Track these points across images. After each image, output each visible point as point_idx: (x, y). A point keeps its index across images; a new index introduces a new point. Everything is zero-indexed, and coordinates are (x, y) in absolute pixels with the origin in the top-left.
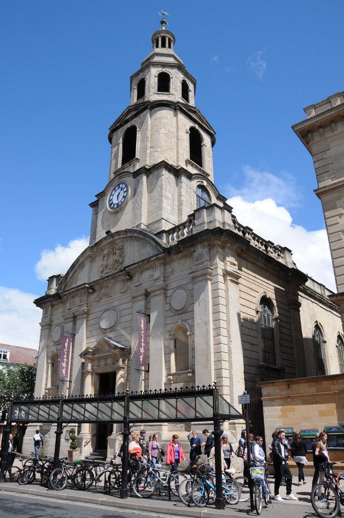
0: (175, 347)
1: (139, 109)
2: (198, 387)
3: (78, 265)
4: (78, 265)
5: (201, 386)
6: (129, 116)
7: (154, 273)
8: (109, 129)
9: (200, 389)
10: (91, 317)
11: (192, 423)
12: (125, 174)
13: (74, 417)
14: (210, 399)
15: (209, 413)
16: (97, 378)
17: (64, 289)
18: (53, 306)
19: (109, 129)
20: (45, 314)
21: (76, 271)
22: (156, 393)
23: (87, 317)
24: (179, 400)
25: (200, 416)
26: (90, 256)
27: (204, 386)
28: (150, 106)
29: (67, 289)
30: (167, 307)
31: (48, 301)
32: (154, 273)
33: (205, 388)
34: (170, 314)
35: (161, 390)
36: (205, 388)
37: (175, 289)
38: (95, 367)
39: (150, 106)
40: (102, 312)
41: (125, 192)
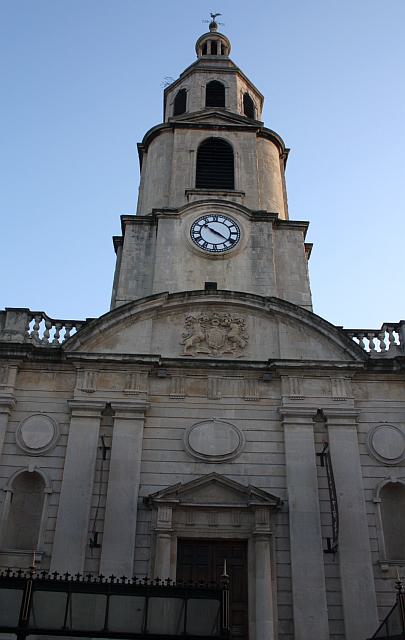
5: (73, 574)
7: (334, 388)
9: (104, 581)
10: (152, 422)
17: (78, 348)
40: (193, 422)
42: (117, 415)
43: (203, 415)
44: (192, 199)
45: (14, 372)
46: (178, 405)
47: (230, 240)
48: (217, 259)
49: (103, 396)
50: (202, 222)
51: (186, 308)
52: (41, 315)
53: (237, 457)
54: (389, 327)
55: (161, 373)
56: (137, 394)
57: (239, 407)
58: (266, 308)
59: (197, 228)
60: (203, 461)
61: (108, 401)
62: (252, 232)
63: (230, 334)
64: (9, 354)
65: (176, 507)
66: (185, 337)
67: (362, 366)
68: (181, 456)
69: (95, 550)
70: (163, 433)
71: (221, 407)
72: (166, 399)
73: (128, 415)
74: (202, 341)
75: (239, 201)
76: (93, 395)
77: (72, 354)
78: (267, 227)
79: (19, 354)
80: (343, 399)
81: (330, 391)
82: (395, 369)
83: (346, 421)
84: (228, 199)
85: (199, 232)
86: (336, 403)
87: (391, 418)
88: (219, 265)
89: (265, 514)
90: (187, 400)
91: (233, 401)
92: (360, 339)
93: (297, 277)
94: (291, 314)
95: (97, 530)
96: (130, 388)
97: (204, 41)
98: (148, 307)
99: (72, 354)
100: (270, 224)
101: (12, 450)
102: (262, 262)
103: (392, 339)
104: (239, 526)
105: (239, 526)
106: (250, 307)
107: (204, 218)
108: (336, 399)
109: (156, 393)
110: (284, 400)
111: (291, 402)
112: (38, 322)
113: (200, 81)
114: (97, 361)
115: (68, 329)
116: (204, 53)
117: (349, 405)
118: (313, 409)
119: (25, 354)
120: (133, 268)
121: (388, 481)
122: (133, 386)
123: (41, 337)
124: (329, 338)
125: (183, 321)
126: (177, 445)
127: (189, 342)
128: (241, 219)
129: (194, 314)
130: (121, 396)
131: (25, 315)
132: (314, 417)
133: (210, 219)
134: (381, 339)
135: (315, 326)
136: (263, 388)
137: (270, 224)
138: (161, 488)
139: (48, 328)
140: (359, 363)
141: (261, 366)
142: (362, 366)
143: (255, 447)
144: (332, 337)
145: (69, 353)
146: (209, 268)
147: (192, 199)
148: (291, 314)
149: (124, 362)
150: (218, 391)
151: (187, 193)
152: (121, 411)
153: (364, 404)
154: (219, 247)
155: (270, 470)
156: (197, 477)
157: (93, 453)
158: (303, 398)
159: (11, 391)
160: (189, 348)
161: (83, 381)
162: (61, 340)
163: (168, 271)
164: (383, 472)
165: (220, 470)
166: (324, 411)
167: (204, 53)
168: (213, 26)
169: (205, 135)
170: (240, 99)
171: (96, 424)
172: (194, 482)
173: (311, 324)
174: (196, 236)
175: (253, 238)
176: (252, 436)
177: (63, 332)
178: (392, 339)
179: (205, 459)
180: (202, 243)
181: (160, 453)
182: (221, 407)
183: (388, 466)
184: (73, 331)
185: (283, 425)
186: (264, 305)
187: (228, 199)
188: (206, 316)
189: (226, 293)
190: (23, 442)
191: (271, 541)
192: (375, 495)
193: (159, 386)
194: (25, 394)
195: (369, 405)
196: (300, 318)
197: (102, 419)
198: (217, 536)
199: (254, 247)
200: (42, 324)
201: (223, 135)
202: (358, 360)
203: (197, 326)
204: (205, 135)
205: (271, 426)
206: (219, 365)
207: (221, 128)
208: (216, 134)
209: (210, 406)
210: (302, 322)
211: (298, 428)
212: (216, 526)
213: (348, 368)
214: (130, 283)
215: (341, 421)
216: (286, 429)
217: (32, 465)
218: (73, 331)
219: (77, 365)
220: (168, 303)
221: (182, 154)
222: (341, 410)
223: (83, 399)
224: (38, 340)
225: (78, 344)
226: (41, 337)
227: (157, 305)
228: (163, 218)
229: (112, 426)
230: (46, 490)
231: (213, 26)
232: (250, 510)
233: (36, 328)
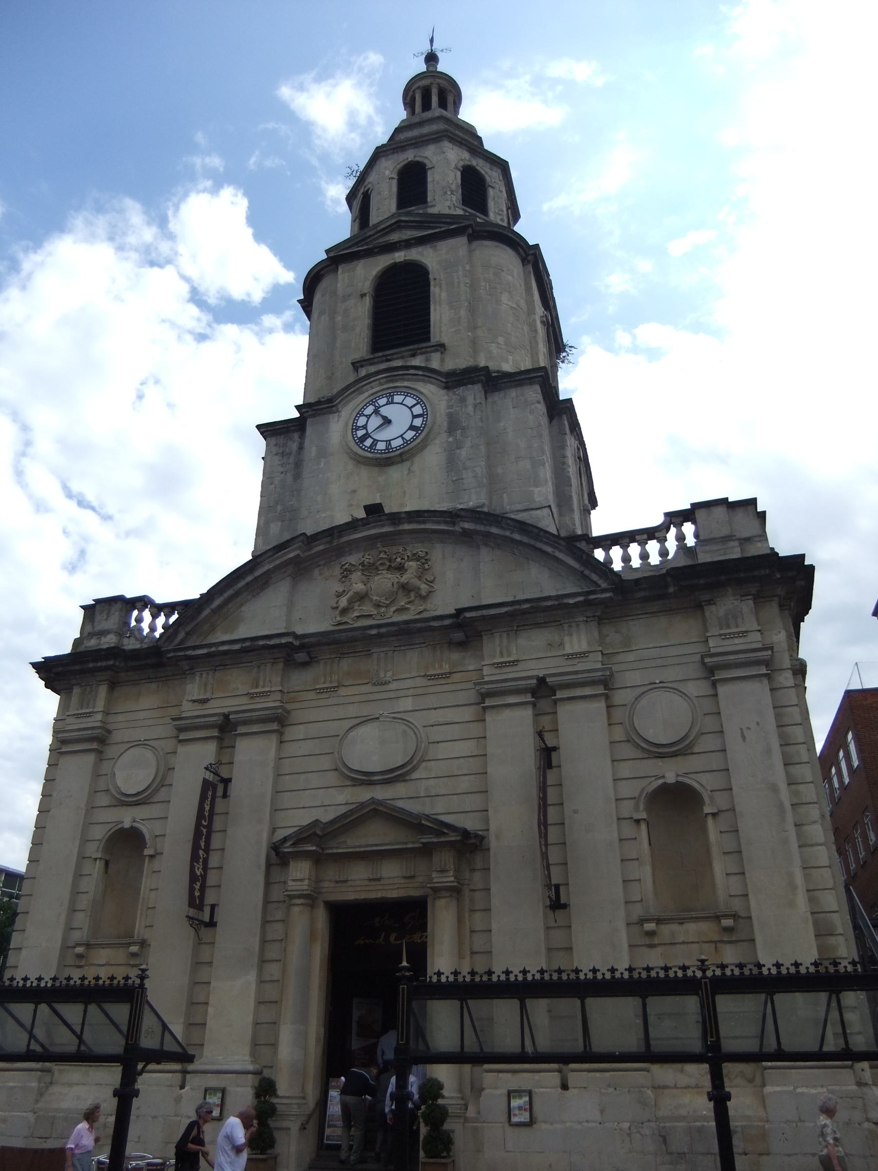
0: (650, 844)
1: (460, 223)
2: (439, 974)
3: (249, 579)
4: (249, 579)
5: (33, 977)
6: (395, 237)
7: (567, 639)
8: (327, 251)
9: (28, 984)
10: (292, 733)
11: (486, 1066)
12: (412, 372)
13: (37, 1041)
14: (121, 1012)
15: (115, 1044)
16: (321, 917)
17: (182, 641)
18: (113, 685)
19: (327, 251)
20: (63, 707)
21: (237, 594)
22: (38, 985)
23: (280, 733)
24: (93, 1008)
25: (38, 1049)
26: (296, 562)
27: (797, 965)
28: (470, 231)
29: (189, 644)
30: (619, 733)
31: (106, 668)
32: (567, 639)
33: (43, 984)
34: (627, 751)
35: (490, 973)
36: (460, 979)
37: (646, 688)
38: (326, 884)
39: (470, 231)
40: (348, 724)
41: (415, 417)
42: (559, 695)
43: (366, 710)
44: (363, 372)
45: (103, 691)
46: (331, 701)
47: (412, 428)
48: (392, 464)
49: (221, 705)
50: (370, 410)
51: (340, 551)
52: (143, 602)
53: (414, 769)
54: (676, 518)
55: (301, 657)
56: (744, 634)
57: (420, 691)
58: (457, 528)
59: (362, 421)
60: (362, 783)
61: (226, 711)
62: (450, 407)
63: (404, 579)
64: (91, 665)
65: (318, 859)
66: (339, 595)
67: (608, 595)
68: (332, 778)
69: (560, 913)
70: (306, 747)
71: (392, 695)
72: (312, 695)
73: (255, 728)
74: (362, 597)
75: (435, 363)
76: (207, 706)
77: (175, 650)
78: (473, 393)
79: (104, 664)
80: (583, 655)
81: (561, 645)
82: (671, 590)
83: (588, 691)
84: (417, 361)
85: (365, 427)
86: (727, 642)
87: (670, 675)
88: (396, 473)
89: (446, 858)
90: (342, 691)
91: (409, 683)
92: (607, 549)
93: (526, 464)
94: (494, 530)
95: (554, 881)
96: (257, 687)
97: (411, 93)
98: (278, 562)
99: (175, 650)
100: (478, 387)
101: (103, 800)
102: (464, 453)
103: (681, 538)
104: (413, 877)
105: (413, 877)
106: (434, 531)
107: (372, 402)
108: (570, 656)
109: (298, 688)
110: (486, 671)
111: (498, 671)
112: (141, 611)
113: (389, 168)
114: (209, 655)
115: (167, 616)
116: (426, 106)
117: (594, 662)
118: (528, 678)
119: (111, 662)
120: (277, 503)
121: (660, 781)
122: (261, 683)
123: (146, 630)
124: (557, 559)
125: (337, 571)
126: (326, 763)
127: (343, 602)
128: (429, 389)
129: (353, 559)
130: (244, 700)
131: (119, 605)
132: (534, 692)
133: (383, 401)
134: (662, 540)
135: (532, 542)
136: (456, 656)
137: (478, 387)
138: (291, 831)
139: (155, 616)
140: (604, 591)
141: (447, 622)
142: (608, 595)
143: (442, 751)
144: (558, 554)
145: (169, 651)
146: (381, 479)
147: (363, 372)
148: (494, 530)
149: (511, 615)
150: (386, 671)
151: (357, 365)
152: (245, 722)
153: (621, 657)
154: (395, 444)
155: (465, 784)
156: (354, 806)
157: (530, 761)
158: (515, 663)
159: (278, 696)
160: (344, 611)
161: (193, 689)
162: (159, 631)
163: (319, 498)
164: (652, 767)
165: (381, 793)
166: (548, 680)
167: (426, 106)
168: (431, 58)
169: (383, 262)
170: (454, 179)
171: (527, 713)
172: (344, 816)
173: (526, 540)
174: (360, 433)
175: (450, 416)
176: (437, 734)
177: (161, 621)
178: (681, 538)
179: (366, 779)
180: (368, 442)
181: (303, 776)
182: (392, 695)
183: (661, 756)
184: (175, 617)
185: (714, 684)
186: (454, 524)
187: (417, 361)
188: (368, 558)
189: (395, 518)
190: (117, 788)
191: (640, 883)
192: (636, 808)
193: (300, 679)
194: (120, 718)
195: (631, 657)
196: (508, 533)
197: (534, 705)
198: (379, 895)
199: (451, 431)
200: (147, 615)
201: (414, 254)
202: (604, 585)
203: (356, 576)
204: (383, 262)
205: (467, 714)
206: (383, 630)
207: (407, 244)
208: (400, 256)
209: (372, 697)
210: (513, 540)
211: (507, 714)
212: (379, 879)
213: (587, 603)
214: (272, 525)
215: (579, 692)
216: (722, 690)
217: (127, 818)
218: (175, 617)
219: (185, 665)
220: (310, 550)
221: (351, 302)
222: (576, 673)
223: (76, 727)
224: (142, 639)
225: (181, 635)
226: (146, 630)
227: (291, 555)
228: (313, 416)
229: (556, 713)
230: (707, 810)
231: (431, 58)
232: (426, 851)
233: (139, 620)
